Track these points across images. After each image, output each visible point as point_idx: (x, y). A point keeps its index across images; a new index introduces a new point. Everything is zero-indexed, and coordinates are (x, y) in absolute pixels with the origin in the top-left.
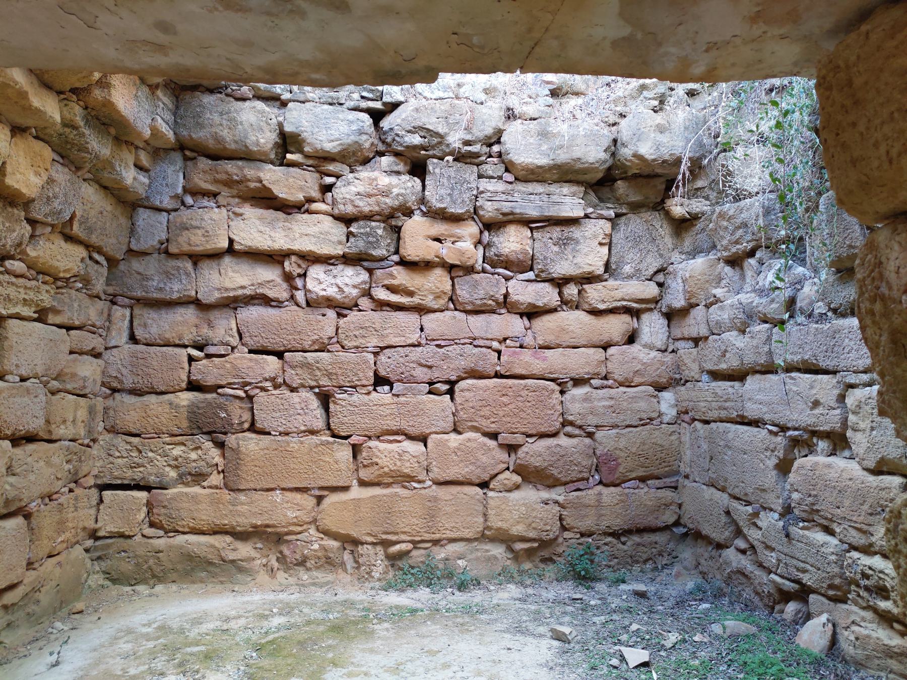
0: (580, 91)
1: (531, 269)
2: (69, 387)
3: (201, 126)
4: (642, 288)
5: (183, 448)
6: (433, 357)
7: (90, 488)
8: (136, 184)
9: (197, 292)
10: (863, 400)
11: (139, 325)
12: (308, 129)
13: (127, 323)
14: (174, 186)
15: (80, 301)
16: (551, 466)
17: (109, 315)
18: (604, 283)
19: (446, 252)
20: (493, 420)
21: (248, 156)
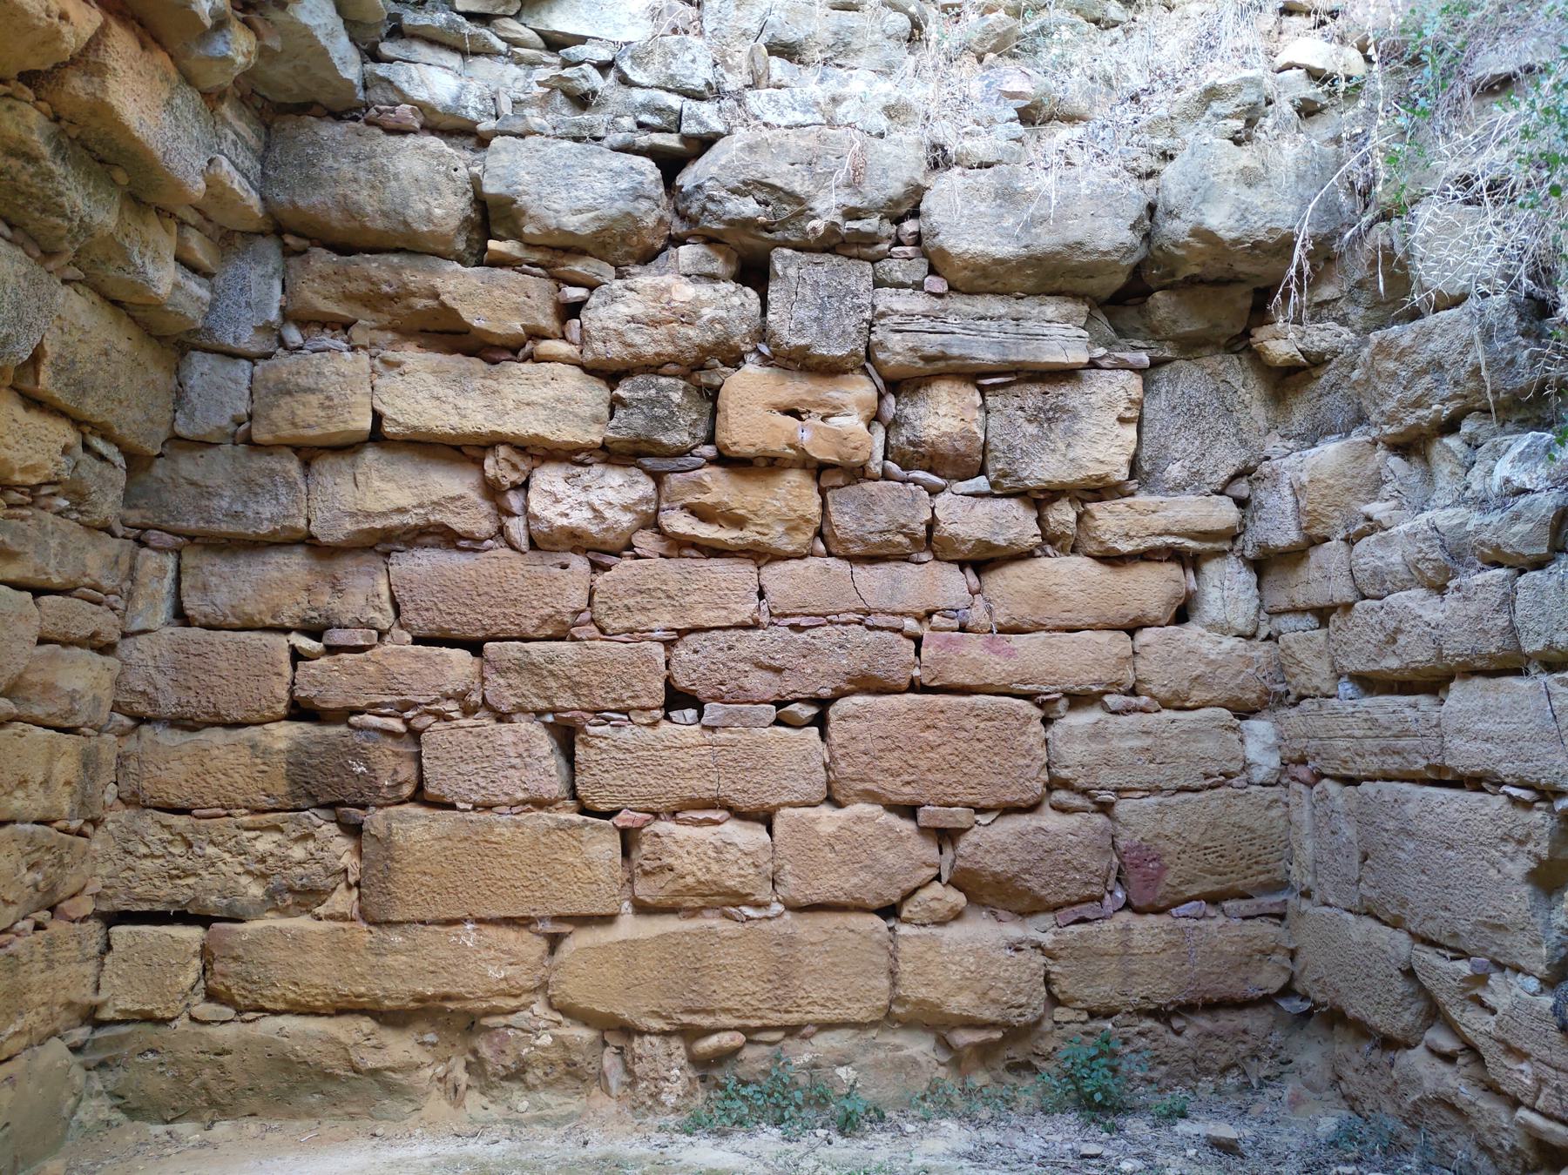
0: (1077, 112)
1: (982, 471)
2: (38, 711)
3: (314, 182)
4: (1205, 510)
5: (277, 837)
6: (783, 650)
7: (84, 919)
8: (180, 298)
9: (309, 521)
11: (193, 587)
12: (532, 189)
13: (168, 582)
14: (262, 306)
15: (65, 536)
17: (132, 568)
18: (1128, 500)
19: (811, 436)
20: (906, 778)
21: (409, 244)
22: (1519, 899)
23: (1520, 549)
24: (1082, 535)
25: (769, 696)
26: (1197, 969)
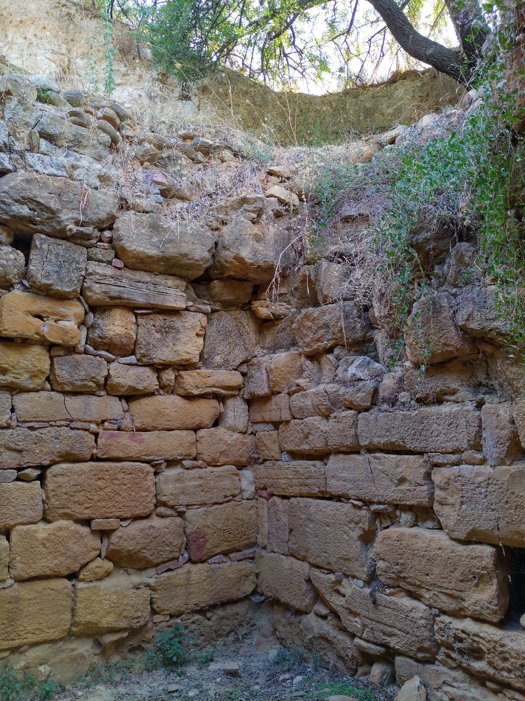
0: (185, 196)
1: (133, 353)
4: (229, 377)
6: (24, 440)
10: (452, 477)
16: (144, 548)
18: (198, 371)
19: (48, 329)
20: (87, 505)
22: (355, 547)
23: (360, 403)
24: (177, 385)
25: (14, 465)
26: (219, 588)
